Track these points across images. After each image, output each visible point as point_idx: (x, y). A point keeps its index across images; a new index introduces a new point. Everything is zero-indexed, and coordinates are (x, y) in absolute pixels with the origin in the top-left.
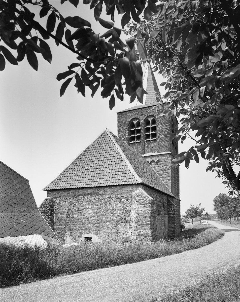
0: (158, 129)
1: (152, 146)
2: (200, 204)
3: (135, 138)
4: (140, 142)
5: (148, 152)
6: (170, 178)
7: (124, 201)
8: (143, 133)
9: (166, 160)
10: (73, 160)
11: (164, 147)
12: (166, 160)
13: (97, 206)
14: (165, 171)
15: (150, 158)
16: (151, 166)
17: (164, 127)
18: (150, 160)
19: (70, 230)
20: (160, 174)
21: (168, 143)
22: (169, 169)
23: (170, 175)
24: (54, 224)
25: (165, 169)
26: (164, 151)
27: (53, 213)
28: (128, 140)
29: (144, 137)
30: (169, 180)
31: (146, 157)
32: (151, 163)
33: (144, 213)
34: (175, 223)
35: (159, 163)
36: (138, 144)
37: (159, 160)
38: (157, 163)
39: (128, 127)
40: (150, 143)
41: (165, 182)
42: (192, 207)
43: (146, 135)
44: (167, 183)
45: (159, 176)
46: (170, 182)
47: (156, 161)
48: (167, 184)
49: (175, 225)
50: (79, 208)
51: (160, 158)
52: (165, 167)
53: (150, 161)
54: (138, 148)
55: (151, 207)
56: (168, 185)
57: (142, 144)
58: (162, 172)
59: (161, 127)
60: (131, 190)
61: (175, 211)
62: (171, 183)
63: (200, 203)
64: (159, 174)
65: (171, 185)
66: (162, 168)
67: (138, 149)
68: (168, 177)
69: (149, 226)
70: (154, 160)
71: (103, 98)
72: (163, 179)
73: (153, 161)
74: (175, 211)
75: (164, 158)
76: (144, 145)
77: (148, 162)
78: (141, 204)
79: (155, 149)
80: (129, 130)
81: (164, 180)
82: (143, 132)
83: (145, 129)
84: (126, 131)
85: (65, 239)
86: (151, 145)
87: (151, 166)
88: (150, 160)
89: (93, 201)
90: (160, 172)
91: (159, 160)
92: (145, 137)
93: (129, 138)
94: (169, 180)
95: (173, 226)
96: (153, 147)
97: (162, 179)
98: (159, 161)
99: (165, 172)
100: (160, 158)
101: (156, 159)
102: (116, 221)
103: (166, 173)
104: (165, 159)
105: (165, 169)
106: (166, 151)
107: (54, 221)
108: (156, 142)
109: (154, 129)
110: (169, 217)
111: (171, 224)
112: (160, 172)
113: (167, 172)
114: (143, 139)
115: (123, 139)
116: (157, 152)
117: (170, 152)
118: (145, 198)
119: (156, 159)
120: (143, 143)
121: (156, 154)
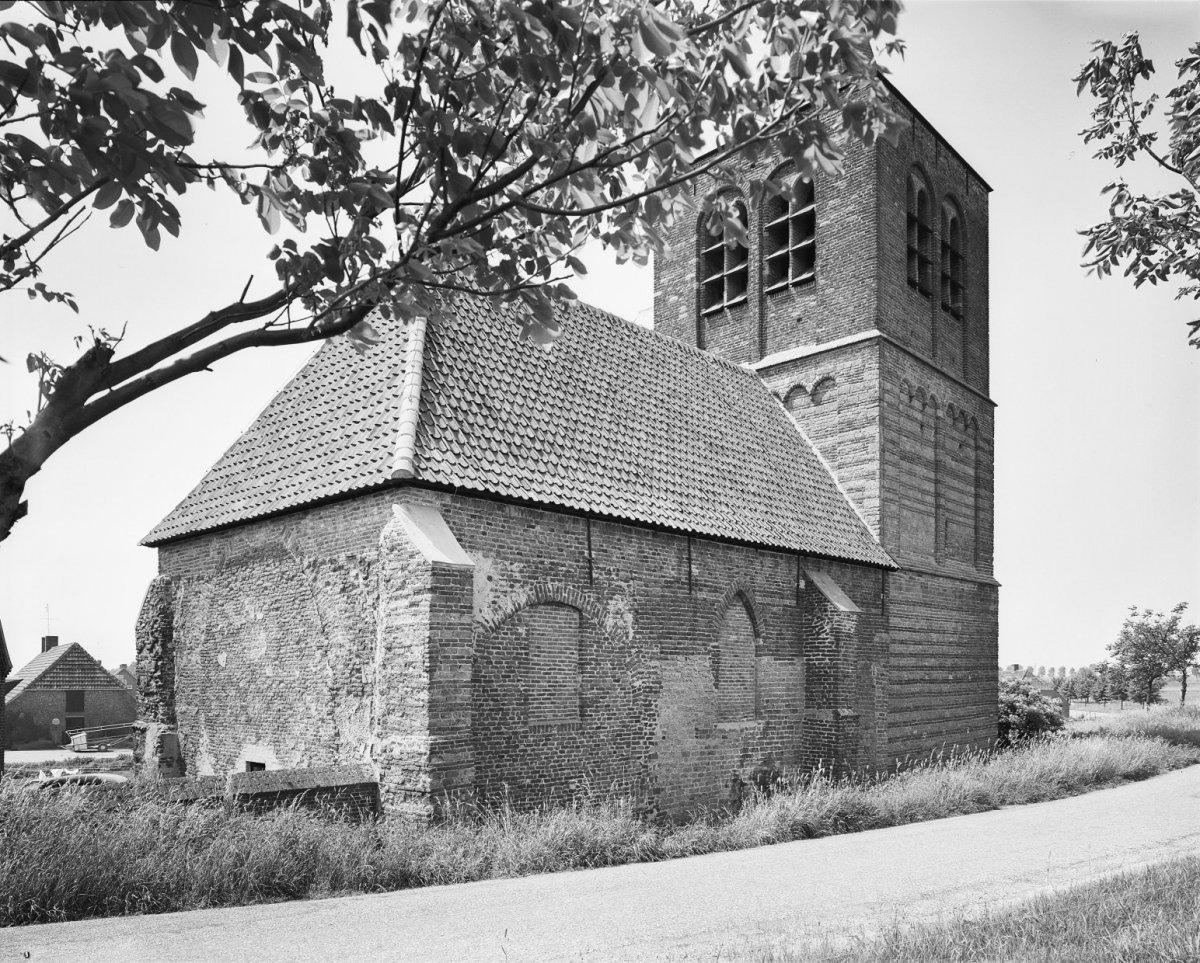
0: (821, 222)
1: (795, 315)
2: (1181, 608)
3: (726, 286)
4: (745, 301)
5: (780, 348)
6: (875, 466)
7: (356, 582)
8: (757, 258)
9: (855, 377)
10: (995, 472)
11: (851, 308)
12: (855, 377)
13: (277, 609)
14: (852, 435)
15: (785, 375)
16: (791, 417)
17: (851, 208)
18: (782, 383)
19: (211, 723)
20: (830, 453)
21: (868, 286)
22: (870, 422)
23: (874, 448)
24: (172, 695)
25: (850, 425)
26: (850, 333)
27: (169, 645)
28: (694, 301)
29: (761, 275)
30: (869, 476)
31: (765, 372)
32: (787, 400)
33: (408, 643)
34: (836, 702)
35: (826, 396)
36: (737, 313)
37: (826, 381)
38: (815, 396)
39: (694, 239)
40: (790, 298)
41: (850, 490)
42: (1137, 620)
43: (771, 261)
44: (859, 495)
45: (826, 465)
46: (873, 487)
47: (809, 388)
48: (860, 501)
49: (837, 714)
50: (231, 621)
51: (826, 367)
52: (849, 414)
53: (783, 391)
54: (735, 334)
55: (431, 606)
56: (866, 502)
57: (754, 309)
58: (837, 438)
59: (834, 208)
60: (376, 519)
61: (838, 640)
62: (877, 493)
63: (1180, 601)
64: (824, 451)
65: (877, 502)
66: (837, 419)
67: (737, 337)
68: (863, 462)
69: (422, 719)
70: (804, 383)
71: (110, 28)
72: (844, 472)
73: (798, 388)
74: (838, 640)
75: (848, 364)
76: (762, 316)
77: (777, 395)
78: (400, 592)
79: (810, 324)
80: (698, 251)
81: (849, 479)
82: (757, 252)
83: (766, 234)
84: (686, 259)
85: (198, 764)
86: (790, 310)
87: (791, 417)
88: (782, 383)
89: (266, 588)
90: (829, 441)
91: (826, 381)
92: (766, 272)
93: (698, 291)
94: (869, 476)
95: (826, 716)
96: (799, 320)
97: (834, 475)
98: (827, 383)
99: (852, 437)
100: (831, 367)
101: (809, 377)
102: (330, 685)
103: (857, 440)
104: (852, 372)
105: (850, 425)
106: (859, 330)
107: (173, 683)
108: (813, 291)
109: (807, 225)
110: (809, 667)
111: (820, 707)
112: (829, 441)
113: (860, 435)
114: (757, 287)
115: (676, 298)
116: (819, 341)
117: (875, 333)
118: (411, 560)
119: (809, 377)
120: (757, 303)
121: (813, 348)
